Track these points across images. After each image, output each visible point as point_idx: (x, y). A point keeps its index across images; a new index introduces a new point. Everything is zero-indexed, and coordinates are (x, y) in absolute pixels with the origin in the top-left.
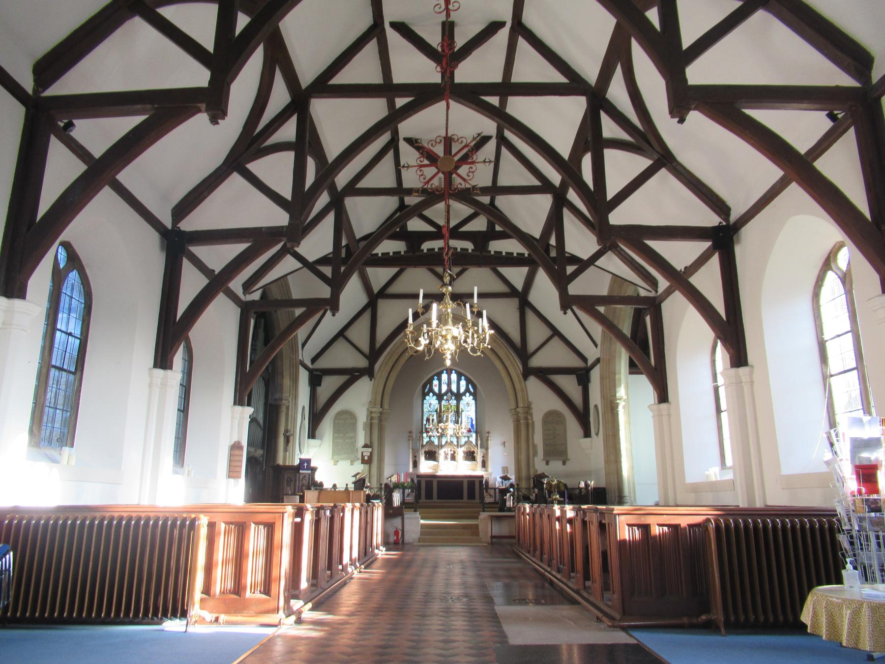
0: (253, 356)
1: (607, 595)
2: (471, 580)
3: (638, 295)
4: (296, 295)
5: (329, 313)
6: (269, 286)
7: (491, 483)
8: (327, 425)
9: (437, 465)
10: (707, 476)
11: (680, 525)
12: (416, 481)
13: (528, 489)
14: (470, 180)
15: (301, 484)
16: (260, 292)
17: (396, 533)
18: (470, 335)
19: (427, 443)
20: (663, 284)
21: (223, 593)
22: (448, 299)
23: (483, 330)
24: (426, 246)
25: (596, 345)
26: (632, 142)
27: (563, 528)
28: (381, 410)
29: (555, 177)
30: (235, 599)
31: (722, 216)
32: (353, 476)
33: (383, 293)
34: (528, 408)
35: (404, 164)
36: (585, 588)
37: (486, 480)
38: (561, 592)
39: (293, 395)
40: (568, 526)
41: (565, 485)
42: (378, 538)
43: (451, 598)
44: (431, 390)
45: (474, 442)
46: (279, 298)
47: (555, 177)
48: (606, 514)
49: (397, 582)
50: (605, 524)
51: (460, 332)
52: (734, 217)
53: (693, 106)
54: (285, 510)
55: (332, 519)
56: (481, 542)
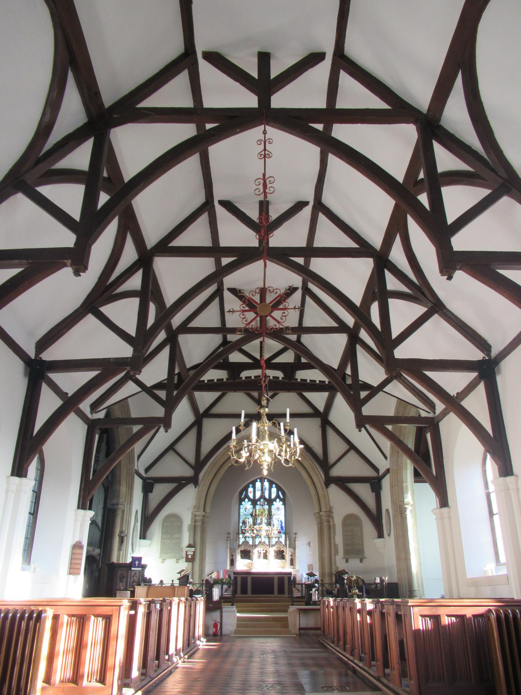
0: (95, 467)
1: (405, 681)
2: (283, 669)
3: (419, 415)
4: (134, 414)
5: (162, 430)
6: (112, 407)
7: (298, 579)
8: (156, 527)
9: (251, 563)
10: (485, 572)
11: (465, 615)
12: (232, 578)
13: (331, 584)
14: (283, 322)
15: (132, 581)
16: (105, 411)
17: (215, 625)
18: (284, 449)
19: (243, 542)
20: (440, 406)
21: (62, 682)
22: (265, 419)
23: (294, 444)
24: (244, 374)
25: (386, 458)
26: (410, 293)
27: (363, 620)
28: (204, 513)
29: (350, 320)
30: (74, 687)
31: (485, 352)
32: (178, 573)
33: (208, 413)
34: (330, 512)
35: (230, 309)
36: (385, 675)
37: (294, 576)
38: (364, 679)
39: (128, 501)
40: (368, 617)
41: (363, 581)
42: (199, 631)
43: (266, 686)
44: (247, 496)
45: (283, 543)
46: (120, 417)
47: (350, 320)
48: (401, 606)
49: (217, 671)
50: (401, 615)
51: (275, 446)
52: (494, 352)
53: (458, 267)
54: (121, 604)
55: (161, 611)
56: (290, 634)
